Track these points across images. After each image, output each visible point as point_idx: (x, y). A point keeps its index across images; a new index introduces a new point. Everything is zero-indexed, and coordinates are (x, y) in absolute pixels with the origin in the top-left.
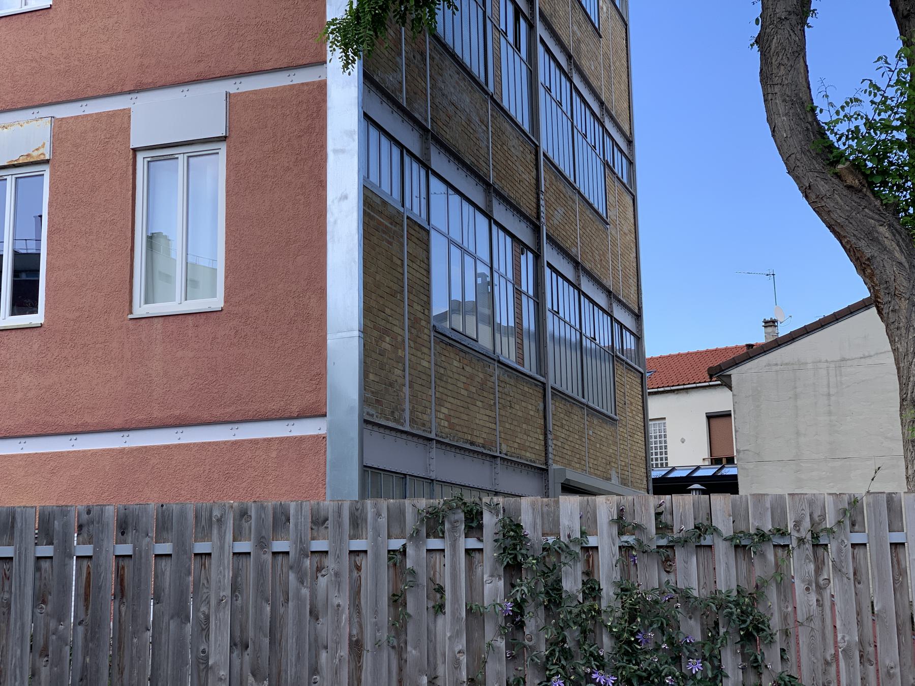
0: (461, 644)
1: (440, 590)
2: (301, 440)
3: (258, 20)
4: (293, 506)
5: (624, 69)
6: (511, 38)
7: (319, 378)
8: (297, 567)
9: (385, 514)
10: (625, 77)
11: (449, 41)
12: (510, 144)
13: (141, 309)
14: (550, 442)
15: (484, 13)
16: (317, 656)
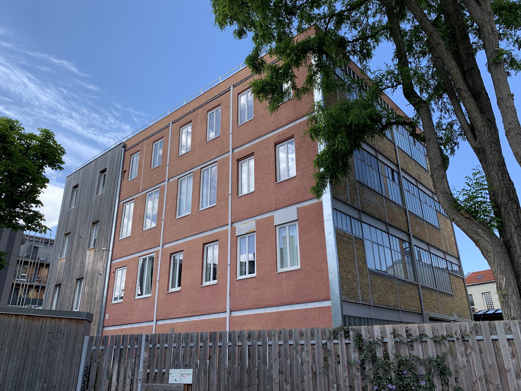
0: (346, 374)
1: (339, 356)
2: (324, 307)
4: (293, 330)
5: (186, 236)
6: (391, 178)
7: (328, 288)
8: (296, 349)
9: (320, 332)
12: (394, 210)
13: (280, 270)
14: (422, 304)
16: (303, 377)
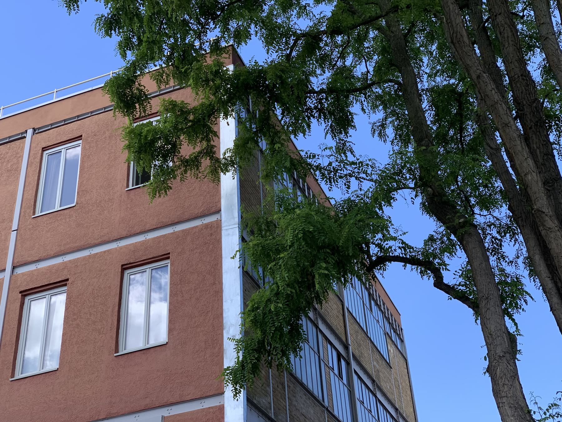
3: (182, 370)
6: (336, 371)
10: (409, 392)
11: (298, 375)
15: (319, 357)
